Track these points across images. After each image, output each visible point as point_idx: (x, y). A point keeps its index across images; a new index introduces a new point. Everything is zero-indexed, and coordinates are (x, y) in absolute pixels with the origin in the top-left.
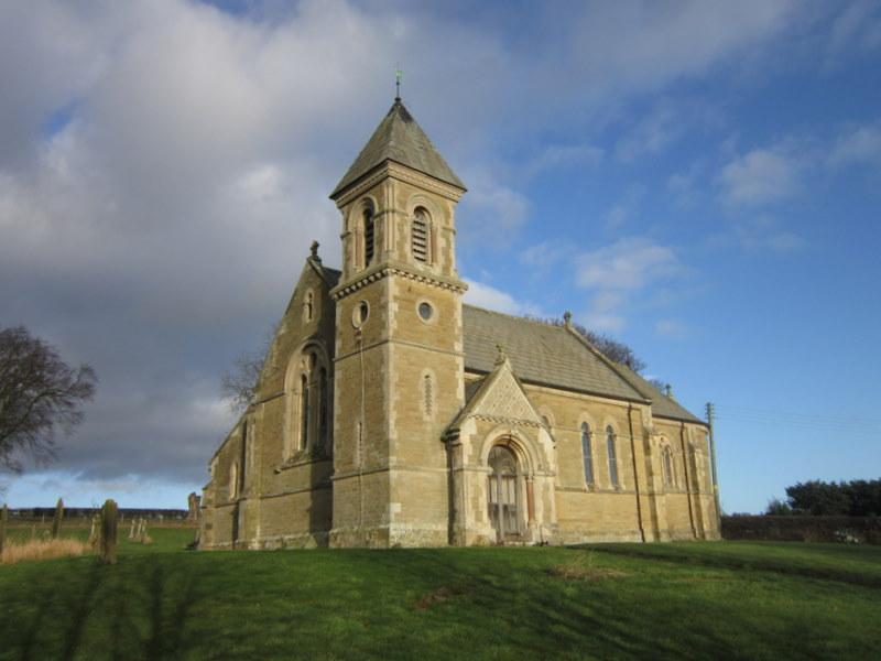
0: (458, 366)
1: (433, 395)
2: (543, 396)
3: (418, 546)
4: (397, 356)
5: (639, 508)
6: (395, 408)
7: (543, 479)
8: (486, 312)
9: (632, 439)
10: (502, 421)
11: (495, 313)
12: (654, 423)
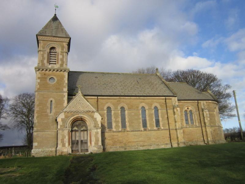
0: (65, 96)
1: (53, 106)
2: (122, 100)
3: (43, 156)
4: (39, 96)
5: (170, 135)
6: (37, 113)
7: (96, 130)
8: (119, 74)
9: (199, 112)
10: (77, 112)
11: (123, 74)
12: (178, 102)
